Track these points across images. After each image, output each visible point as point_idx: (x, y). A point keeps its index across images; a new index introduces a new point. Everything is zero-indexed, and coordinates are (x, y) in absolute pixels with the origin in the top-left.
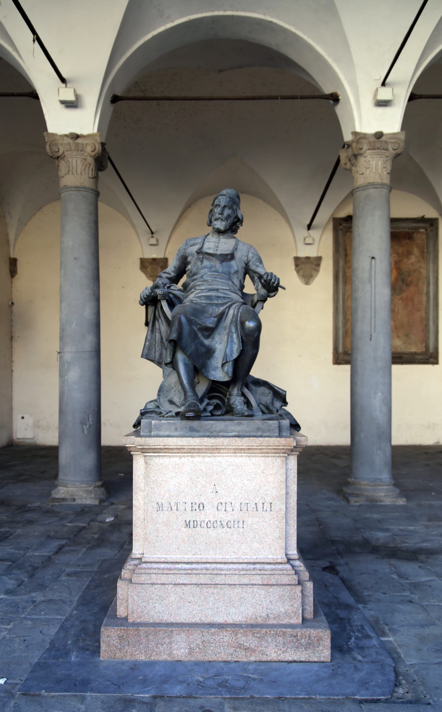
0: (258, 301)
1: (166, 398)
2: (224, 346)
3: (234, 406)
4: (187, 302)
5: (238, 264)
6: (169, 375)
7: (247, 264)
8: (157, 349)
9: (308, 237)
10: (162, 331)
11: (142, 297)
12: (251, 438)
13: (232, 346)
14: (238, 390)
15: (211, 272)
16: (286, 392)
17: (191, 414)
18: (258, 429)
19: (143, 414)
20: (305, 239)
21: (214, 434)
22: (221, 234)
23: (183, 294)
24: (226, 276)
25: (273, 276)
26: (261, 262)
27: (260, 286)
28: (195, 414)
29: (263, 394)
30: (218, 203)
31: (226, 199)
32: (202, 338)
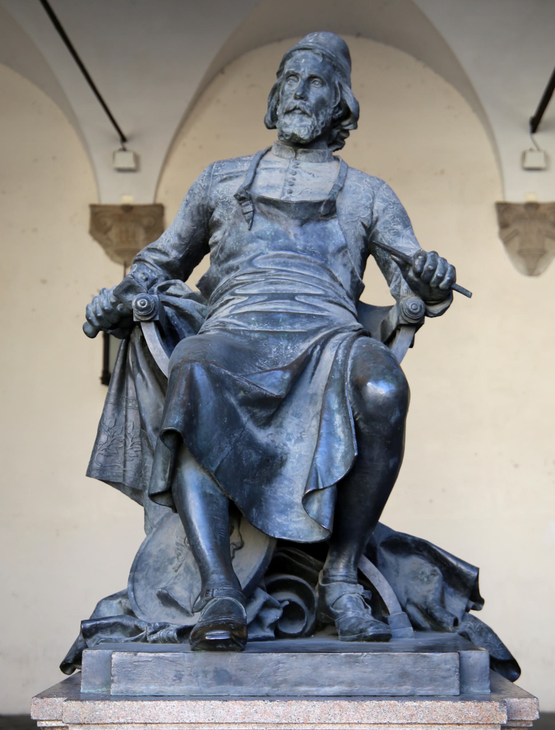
0: (399, 326)
1: (152, 587)
2: (309, 448)
3: (338, 611)
4: (210, 328)
5: (346, 227)
6: (160, 525)
7: (370, 229)
8: (131, 453)
9: (531, 150)
10: (143, 405)
11: (92, 315)
12: (383, 702)
13: (330, 447)
14: (347, 567)
15: (275, 249)
16: (477, 570)
17: (220, 635)
18: (404, 676)
19: (87, 633)
20: (524, 156)
21: (284, 689)
22: (300, 150)
23: (199, 306)
24: (313, 259)
25: (439, 261)
26: (406, 222)
27: (405, 286)
28: (231, 635)
29: (415, 575)
30: (293, 69)
31: (315, 59)
32: (250, 426)
